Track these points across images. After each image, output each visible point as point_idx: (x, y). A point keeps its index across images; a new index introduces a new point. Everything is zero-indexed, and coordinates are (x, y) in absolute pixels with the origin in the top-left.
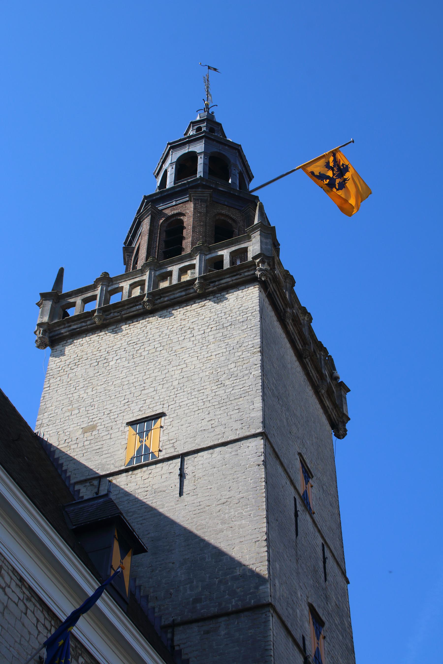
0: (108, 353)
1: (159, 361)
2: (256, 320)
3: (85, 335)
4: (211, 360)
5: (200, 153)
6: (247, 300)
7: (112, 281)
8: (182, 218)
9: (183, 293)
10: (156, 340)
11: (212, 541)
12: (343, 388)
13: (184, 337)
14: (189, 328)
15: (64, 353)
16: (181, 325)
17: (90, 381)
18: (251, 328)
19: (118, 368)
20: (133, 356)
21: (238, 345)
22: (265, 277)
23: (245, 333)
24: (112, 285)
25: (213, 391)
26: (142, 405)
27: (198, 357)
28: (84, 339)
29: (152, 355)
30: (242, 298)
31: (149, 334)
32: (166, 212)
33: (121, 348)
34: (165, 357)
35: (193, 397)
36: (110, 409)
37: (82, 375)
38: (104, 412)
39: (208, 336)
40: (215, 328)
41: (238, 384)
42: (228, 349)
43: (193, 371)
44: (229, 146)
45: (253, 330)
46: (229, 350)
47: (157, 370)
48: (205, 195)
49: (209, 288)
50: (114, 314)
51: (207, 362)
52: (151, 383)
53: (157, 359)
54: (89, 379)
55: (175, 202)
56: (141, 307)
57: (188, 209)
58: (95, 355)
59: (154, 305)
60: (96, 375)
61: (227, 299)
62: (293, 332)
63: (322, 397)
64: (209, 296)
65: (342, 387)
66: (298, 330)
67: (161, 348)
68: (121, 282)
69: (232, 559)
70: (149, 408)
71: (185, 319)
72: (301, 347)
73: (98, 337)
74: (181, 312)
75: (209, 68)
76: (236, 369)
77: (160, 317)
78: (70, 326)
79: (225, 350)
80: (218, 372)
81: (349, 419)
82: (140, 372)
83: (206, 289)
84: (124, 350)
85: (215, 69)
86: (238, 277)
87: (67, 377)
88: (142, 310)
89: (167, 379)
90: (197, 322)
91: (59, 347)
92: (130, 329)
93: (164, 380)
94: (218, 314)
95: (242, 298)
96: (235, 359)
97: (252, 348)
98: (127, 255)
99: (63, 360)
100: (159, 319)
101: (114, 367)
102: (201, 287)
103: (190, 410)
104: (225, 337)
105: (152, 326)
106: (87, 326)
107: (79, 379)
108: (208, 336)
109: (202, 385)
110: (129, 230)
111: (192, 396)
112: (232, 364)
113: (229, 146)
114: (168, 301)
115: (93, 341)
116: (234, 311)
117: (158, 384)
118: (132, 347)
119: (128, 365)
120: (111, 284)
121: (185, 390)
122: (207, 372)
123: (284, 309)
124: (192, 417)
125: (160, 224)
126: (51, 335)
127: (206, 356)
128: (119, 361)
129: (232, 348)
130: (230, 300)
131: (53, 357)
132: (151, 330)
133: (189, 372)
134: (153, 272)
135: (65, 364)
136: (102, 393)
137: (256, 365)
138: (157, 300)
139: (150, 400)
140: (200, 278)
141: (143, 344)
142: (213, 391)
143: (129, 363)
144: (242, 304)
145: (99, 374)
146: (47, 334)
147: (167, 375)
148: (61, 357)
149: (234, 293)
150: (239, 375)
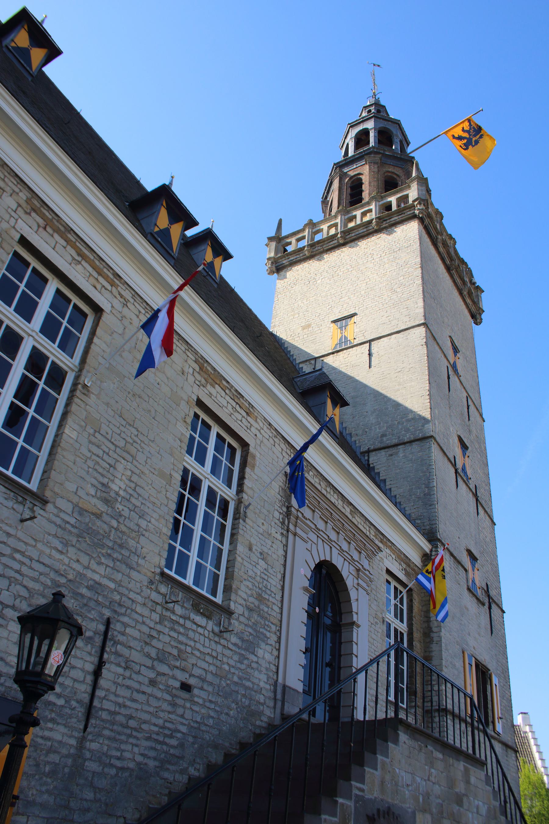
2: (416, 246)
9: (365, 230)
11: (392, 397)
44: (392, 122)
50: (318, 248)
56: (336, 241)
61: (395, 232)
69: (406, 408)
75: (374, 65)
81: (484, 311)
85: (379, 66)
91: (282, 273)
113: (392, 122)
116: (401, 240)
128: (323, 280)
140: (376, 218)
150: (407, 284)
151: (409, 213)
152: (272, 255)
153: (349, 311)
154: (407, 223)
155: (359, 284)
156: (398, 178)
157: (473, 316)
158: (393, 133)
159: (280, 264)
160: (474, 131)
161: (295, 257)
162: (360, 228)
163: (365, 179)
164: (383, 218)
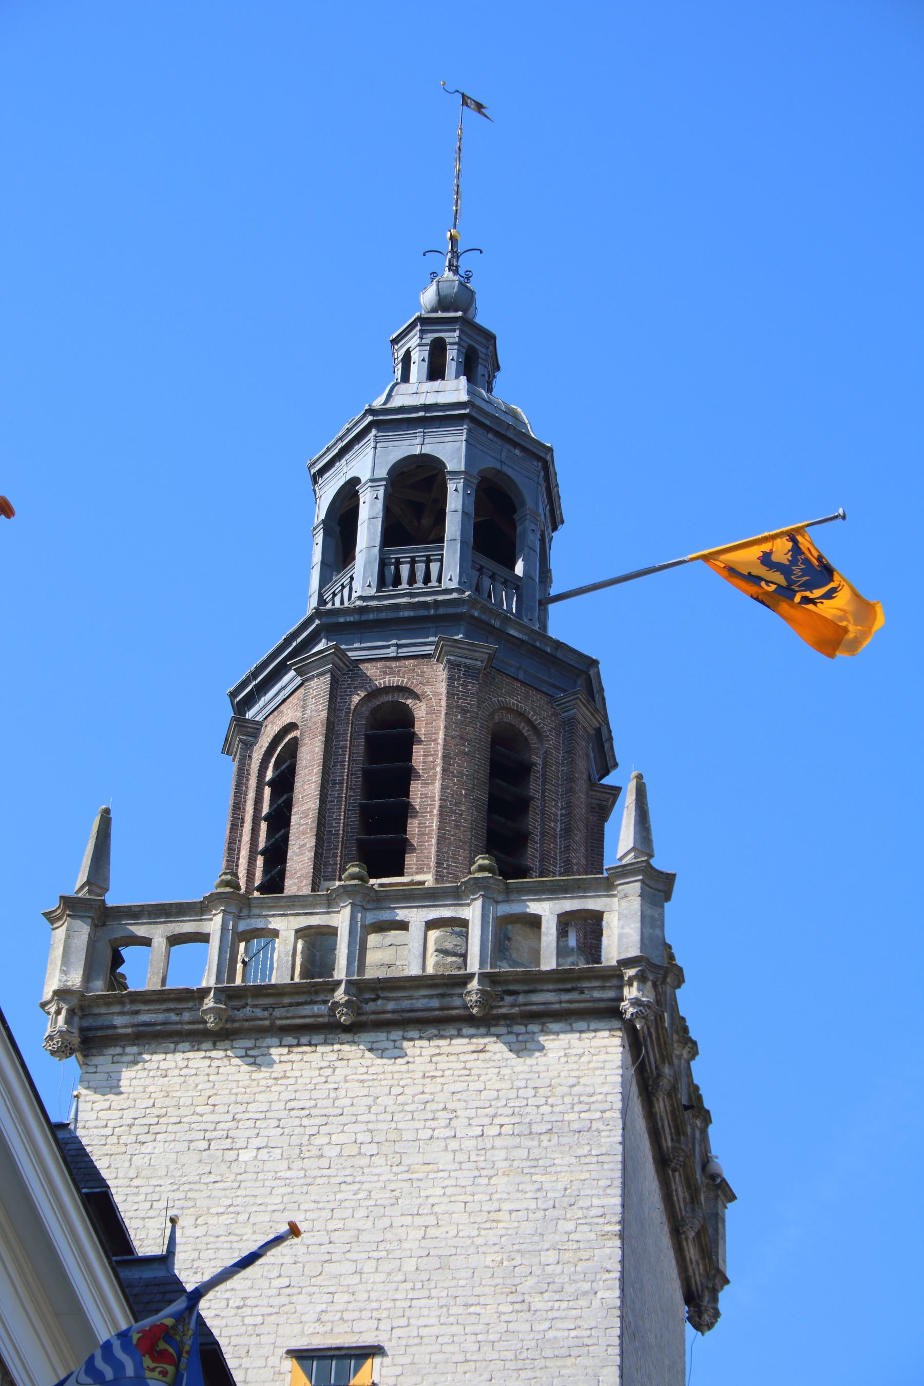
0: (234, 1119)
1: (366, 1186)
3: (172, 1046)
4: (500, 1225)
5: (455, 473)
6: (589, 1064)
7: (250, 907)
8: (409, 702)
9: (435, 1003)
10: (360, 1118)
12: (722, 1191)
13: (430, 1132)
14: (445, 1109)
15: (119, 1086)
16: (423, 1093)
17: (190, 1195)
18: (601, 1159)
19: (261, 1176)
20: (301, 1152)
21: (566, 1199)
22: (643, 1021)
23: (586, 1168)
24: (249, 916)
25: (504, 1318)
26: (323, 1307)
27: (466, 1203)
28: (169, 1056)
29: (350, 1162)
30: (581, 1056)
31: (342, 1093)
32: (371, 670)
33: (269, 1115)
34: (383, 1178)
35: (451, 1319)
36: (243, 1294)
37: (167, 1167)
38: (228, 1299)
39: (493, 1148)
40: (507, 1129)
41: (563, 1314)
42: (542, 1205)
43: (453, 1242)
44: (524, 449)
45: (606, 1166)
46: (544, 1206)
47: (362, 1212)
48: (477, 654)
49: (500, 1007)
50: (251, 1011)
51: (488, 1225)
52: (348, 1247)
53: (363, 1179)
54: (187, 1187)
55: (394, 649)
56: (324, 1009)
57: (427, 684)
58: (201, 1115)
59: (359, 1014)
60: (205, 1179)
61: (542, 1049)
62: (664, 1114)
63: (684, 1243)
64: (495, 1025)
65: (720, 1193)
66: (672, 1105)
67: (373, 1148)
68: (273, 915)
70: (342, 1319)
71: (433, 1077)
72: (670, 1144)
73: (207, 1062)
74: (425, 1052)
75: (465, 99)
76: (559, 1268)
77: (370, 1050)
78: (137, 1013)
79: (533, 1205)
80: (514, 1263)
81: (727, 1281)
82: (320, 1205)
83: (492, 1008)
84: (276, 1123)
85: (479, 107)
86: (575, 996)
87: (127, 1164)
88: (326, 1020)
89: (388, 1246)
90: (464, 1096)
91: (102, 1061)
92: (293, 1062)
93: (381, 1247)
94: (518, 1089)
95: (581, 1056)
96: (557, 1237)
97: (601, 1220)
98: (241, 740)
99: (114, 1105)
100: (368, 1054)
101: (251, 1168)
102: (481, 1004)
103: (445, 1356)
104: (535, 1163)
105: (348, 1071)
106: (181, 1023)
107: (161, 1177)
108: (493, 1148)
109: (477, 1291)
110: (253, 669)
111: (449, 1315)
112: (551, 1252)
113: (524, 449)
114: (394, 1012)
115: (193, 1071)
116: (559, 1091)
117: (365, 1255)
118: (297, 1122)
119: (288, 1174)
120: (245, 912)
121: (434, 1293)
122: (489, 1258)
123: (657, 1068)
124: (450, 1377)
125: (352, 707)
126: (86, 1024)
127: (486, 1207)
128: (263, 1154)
129: (551, 1203)
130: (551, 1054)
131: (88, 1088)
132: (346, 1081)
133: (443, 1244)
134: (359, 915)
135: (121, 1122)
136: (221, 1239)
137: (608, 1271)
138: (367, 1001)
139: (346, 1297)
140: (482, 976)
141: (325, 1120)
142: (504, 1318)
143: (289, 1168)
144: (579, 1077)
145: (212, 1178)
146: (76, 1019)
147: (388, 1236)
148: (111, 1097)
149: (562, 1036)
150: (569, 1289)
151: (597, 994)
152: (75, 979)
153: (357, 1327)
154: (582, 1025)
155: (398, 1221)
156: (533, 739)
157: (690, 1298)
158: (523, 503)
159: (99, 1022)
160: (804, 572)
161: (160, 1017)
162: (418, 987)
163: (432, 719)
164: (507, 982)
